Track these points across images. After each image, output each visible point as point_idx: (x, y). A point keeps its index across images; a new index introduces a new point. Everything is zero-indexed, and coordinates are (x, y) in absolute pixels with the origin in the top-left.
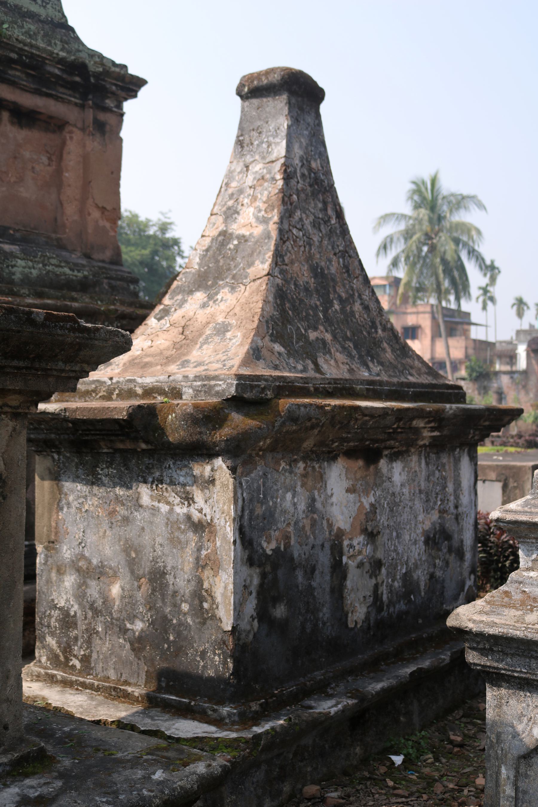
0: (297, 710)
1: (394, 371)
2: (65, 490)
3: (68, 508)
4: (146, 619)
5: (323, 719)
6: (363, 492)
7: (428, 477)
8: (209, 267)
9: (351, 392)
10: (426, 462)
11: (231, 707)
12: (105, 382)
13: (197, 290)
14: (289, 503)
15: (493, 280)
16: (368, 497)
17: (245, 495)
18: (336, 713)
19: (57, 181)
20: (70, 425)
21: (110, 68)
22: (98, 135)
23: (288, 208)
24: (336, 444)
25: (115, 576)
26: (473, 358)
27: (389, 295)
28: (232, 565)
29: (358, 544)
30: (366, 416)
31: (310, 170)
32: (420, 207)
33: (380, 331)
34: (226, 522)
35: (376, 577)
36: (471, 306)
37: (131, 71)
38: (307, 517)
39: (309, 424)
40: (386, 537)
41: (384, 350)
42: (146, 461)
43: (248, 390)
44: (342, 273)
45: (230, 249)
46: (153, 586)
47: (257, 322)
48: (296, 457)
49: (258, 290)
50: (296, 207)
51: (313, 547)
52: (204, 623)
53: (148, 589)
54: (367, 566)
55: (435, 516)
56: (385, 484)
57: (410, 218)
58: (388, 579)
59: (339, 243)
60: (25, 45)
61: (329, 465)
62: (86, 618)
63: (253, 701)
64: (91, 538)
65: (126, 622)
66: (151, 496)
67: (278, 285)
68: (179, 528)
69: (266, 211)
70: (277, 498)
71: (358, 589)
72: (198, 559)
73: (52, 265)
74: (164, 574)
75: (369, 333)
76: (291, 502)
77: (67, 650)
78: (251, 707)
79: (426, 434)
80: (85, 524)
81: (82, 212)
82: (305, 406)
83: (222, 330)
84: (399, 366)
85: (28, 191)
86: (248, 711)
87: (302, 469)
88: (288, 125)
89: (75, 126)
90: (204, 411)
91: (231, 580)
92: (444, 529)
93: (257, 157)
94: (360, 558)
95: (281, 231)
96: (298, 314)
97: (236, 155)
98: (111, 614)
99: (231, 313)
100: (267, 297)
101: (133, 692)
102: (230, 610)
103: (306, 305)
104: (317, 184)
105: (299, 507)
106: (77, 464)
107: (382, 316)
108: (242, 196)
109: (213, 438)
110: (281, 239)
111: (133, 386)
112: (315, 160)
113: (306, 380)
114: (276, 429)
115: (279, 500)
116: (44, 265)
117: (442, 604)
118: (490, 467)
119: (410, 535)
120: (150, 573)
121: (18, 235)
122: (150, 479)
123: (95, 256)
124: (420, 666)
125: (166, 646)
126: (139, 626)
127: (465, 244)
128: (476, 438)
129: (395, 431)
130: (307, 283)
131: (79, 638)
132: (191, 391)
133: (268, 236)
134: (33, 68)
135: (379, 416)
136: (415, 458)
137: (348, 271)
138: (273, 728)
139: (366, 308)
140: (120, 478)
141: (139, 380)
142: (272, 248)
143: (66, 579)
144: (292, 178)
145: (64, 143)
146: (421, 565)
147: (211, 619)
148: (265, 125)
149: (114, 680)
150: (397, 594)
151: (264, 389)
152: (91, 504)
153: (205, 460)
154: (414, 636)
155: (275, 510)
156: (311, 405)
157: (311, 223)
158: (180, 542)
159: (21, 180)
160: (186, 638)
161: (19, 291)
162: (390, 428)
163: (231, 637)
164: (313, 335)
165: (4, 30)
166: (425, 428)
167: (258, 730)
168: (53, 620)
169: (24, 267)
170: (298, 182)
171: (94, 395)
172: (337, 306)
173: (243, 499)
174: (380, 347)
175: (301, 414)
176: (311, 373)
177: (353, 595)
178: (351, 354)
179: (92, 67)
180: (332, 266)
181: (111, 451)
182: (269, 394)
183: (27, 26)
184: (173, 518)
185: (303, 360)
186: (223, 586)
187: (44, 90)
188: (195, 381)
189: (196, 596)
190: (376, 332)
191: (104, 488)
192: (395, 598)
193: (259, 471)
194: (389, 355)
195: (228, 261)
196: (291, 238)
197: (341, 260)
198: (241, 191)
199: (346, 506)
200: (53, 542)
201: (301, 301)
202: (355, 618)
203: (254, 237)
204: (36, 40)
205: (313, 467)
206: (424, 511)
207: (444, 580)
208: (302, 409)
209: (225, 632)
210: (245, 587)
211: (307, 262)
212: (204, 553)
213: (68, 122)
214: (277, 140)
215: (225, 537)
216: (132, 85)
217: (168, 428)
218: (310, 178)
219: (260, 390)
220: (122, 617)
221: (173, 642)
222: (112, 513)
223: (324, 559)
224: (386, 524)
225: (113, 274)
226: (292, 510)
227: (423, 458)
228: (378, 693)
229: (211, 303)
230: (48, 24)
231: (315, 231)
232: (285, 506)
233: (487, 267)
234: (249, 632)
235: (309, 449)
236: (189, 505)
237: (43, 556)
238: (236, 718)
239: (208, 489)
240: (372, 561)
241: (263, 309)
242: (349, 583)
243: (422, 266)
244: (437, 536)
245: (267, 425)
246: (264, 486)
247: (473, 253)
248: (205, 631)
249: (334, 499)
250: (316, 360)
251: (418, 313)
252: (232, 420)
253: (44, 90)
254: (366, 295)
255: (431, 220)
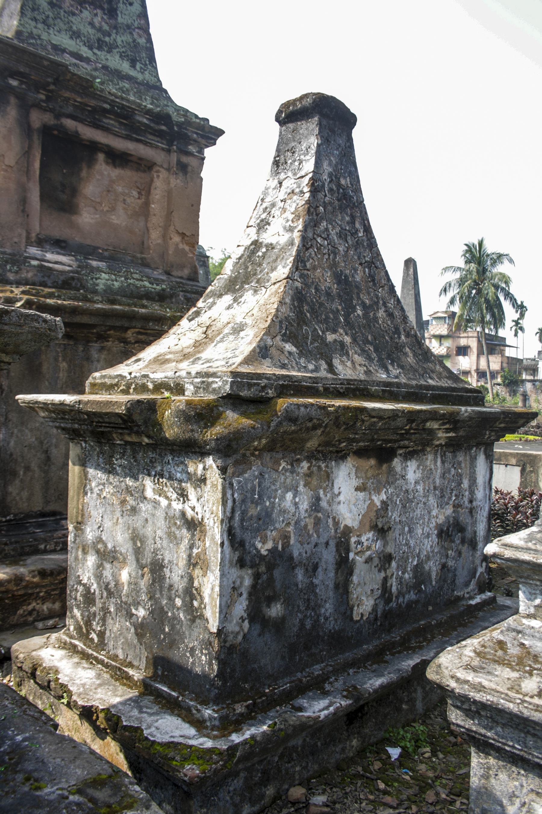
0: (286, 712)
1: (414, 374)
2: (89, 476)
3: (91, 493)
4: (147, 607)
5: (311, 723)
6: (374, 490)
7: (444, 474)
8: (239, 273)
9: (365, 393)
10: (442, 460)
11: (214, 710)
12: (125, 377)
13: (226, 293)
14: (289, 502)
15: (522, 316)
16: (379, 495)
17: (236, 495)
18: (326, 717)
19: (144, 211)
20: (86, 417)
21: (191, 119)
22: (181, 174)
23: (313, 218)
24: (344, 444)
25: (124, 562)
26: (506, 370)
27: (448, 324)
28: (219, 567)
29: (367, 540)
30: (374, 417)
31: (339, 185)
32: (470, 262)
33: (403, 337)
34: (215, 523)
35: (385, 570)
36: (506, 332)
37: (211, 123)
38: (310, 516)
39: (310, 425)
40: (397, 532)
41: (406, 354)
42: (150, 454)
43: (246, 388)
44: (367, 282)
45: (258, 256)
46: (153, 576)
47: (269, 322)
48: (299, 457)
49: (276, 292)
50: (322, 218)
51: (316, 545)
52: (193, 621)
53: (149, 579)
54: (376, 561)
55: (449, 510)
56: (398, 482)
57: (463, 270)
58: (398, 571)
59: (365, 255)
60: (116, 97)
61: (338, 465)
62: (102, 597)
63: (239, 702)
64: (108, 524)
65: (132, 607)
66: (154, 489)
67: (297, 288)
68: (176, 524)
69: (293, 221)
70: (275, 498)
71: (365, 584)
72: (190, 556)
73: (134, 279)
74: (162, 567)
75: (391, 338)
76: (292, 501)
77: (88, 623)
78: (234, 710)
79: (441, 434)
80: (103, 509)
81: (165, 236)
82: (306, 406)
83: (238, 329)
84: (420, 370)
85: (120, 219)
86: (232, 714)
87: (306, 468)
88: (317, 144)
89: (161, 166)
90: (196, 409)
91: (218, 582)
92: (458, 522)
93: (290, 174)
94: (368, 553)
95: (304, 239)
96: (317, 317)
97: (272, 174)
98: (121, 597)
99: (249, 314)
100: (283, 298)
101: (133, 675)
102: (216, 612)
103: (327, 308)
104: (345, 199)
105: (301, 507)
106: (98, 453)
107: (406, 323)
108: (274, 209)
109: (204, 437)
110: (304, 246)
111: (146, 381)
112: (345, 178)
113: (315, 380)
114: (271, 429)
115: (277, 500)
116: (126, 279)
117: (453, 591)
118: (511, 454)
119: (423, 530)
120: (151, 564)
121: (106, 254)
122: (153, 473)
123: (174, 273)
124: (424, 658)
125: (162, 636)
126: (141, 613)
127: (503, 289)
128: (492, 438)
129: (407, 432)
130: (329, 288)
131: (97, 614)
132: (192, 387)
133: (292, 244)
134: (125, 118)
135: (389, 418)
136: (430, 457)
137: (373, 280)
138: (253, 737)
139: (391, 315)
140: (130, 469)
141: (152, 376)
142: (294, 253)
143: (88, 559)
144: (319, 192)
145: (152, 181)
146: (433, 556)
147: (200, 619)
148: (298, 145)
149: (121, 660)
150: (407, 585)
151: (264, 388)
152: (109, 490)
153: (198, 458)
154: (422, 622)
155: (273, 510)
156: (312, 405)
157: (337, 233)
158: (176, 538)
159: (113, 209)
160: (178, 632)
161: (93, 298)
162: (402, 429)
163: (217, 638)
164: (330, 337)
165: (97, 84)
166: (439, 429)
167: (236, 738)
168: (79, 594)
169: (107, 280)
170: (326, 196)
171: (116, 388)
172: (359, 312)
173: (234, 501)
174: (401, 351)
175: (301, 414)
176: (323, 373)
177: (359, 589)
178: (370, 357)
179: (175, 117)
180: (358, 274)
181: (122, 442)
182: (271, 393)
183: (121, 84)
184: (171, 513)
185: (316, 360)
186: (210, 585)
187: (134, 136)
188: (196, 377)
189: (187, 593)
190: (399, 338)
191: (118, 477)
192: (405, 589)
193: (254, 471)
194: (411, 359)
195: (256, 267)
196: (314, 246)
197: (367, 270)
198: (273, 205)
199: (354, 504)
200: (80, 523)
201: (321, 305)
202: (361, 611)
203: (280, 245)
204: (129, 95)
205: (319, 467)
206: (438, 506)
207: (455, 569)
208: (302, 409)
209: (211, 633)
210: (234, 588)
211: (331, 269)
212: (195, 551)
213: (155, 164)
214: (308, 157)
215: (213, 539)
216: (211, 134)
217: (165, 424)
218: (338, 193)
219: (260, 388)
220: (129, 602)
221: (169, 633)
222: (123, 502)
223: (329, 557)
224: (398, 519)
225: (189, 288)
226: (292, 509)
227: (439, 457)
228: (376, 691)
229: (235, 305)
230: (143, 86)
231: (341, 242)
232: (285, 506)
233: (518, 306)
234: (238, 633)
235: (314, 449)
236: (184, 502)
237: (73, 535)
238: (217, 723)
239: (200, 487)
240: (381, 555)
241: (277, 310)
242: (355, 579)
243: (471, 304)
244: (451, 529)
245: (261, 425)
246: (259, 486)
247: (508, 295)
248: (195, 629)
249: (341, 498)
250: (331, 361)
251: (468, 337)
252: (225, 419)
253: (134, 136)
254: (391, 304)
255: (478, 272)
